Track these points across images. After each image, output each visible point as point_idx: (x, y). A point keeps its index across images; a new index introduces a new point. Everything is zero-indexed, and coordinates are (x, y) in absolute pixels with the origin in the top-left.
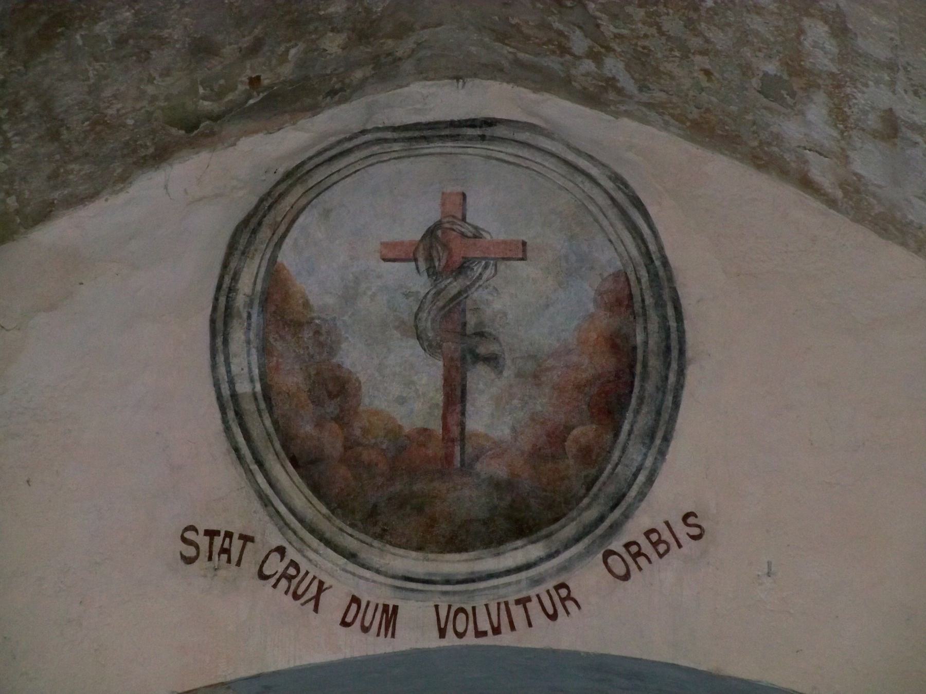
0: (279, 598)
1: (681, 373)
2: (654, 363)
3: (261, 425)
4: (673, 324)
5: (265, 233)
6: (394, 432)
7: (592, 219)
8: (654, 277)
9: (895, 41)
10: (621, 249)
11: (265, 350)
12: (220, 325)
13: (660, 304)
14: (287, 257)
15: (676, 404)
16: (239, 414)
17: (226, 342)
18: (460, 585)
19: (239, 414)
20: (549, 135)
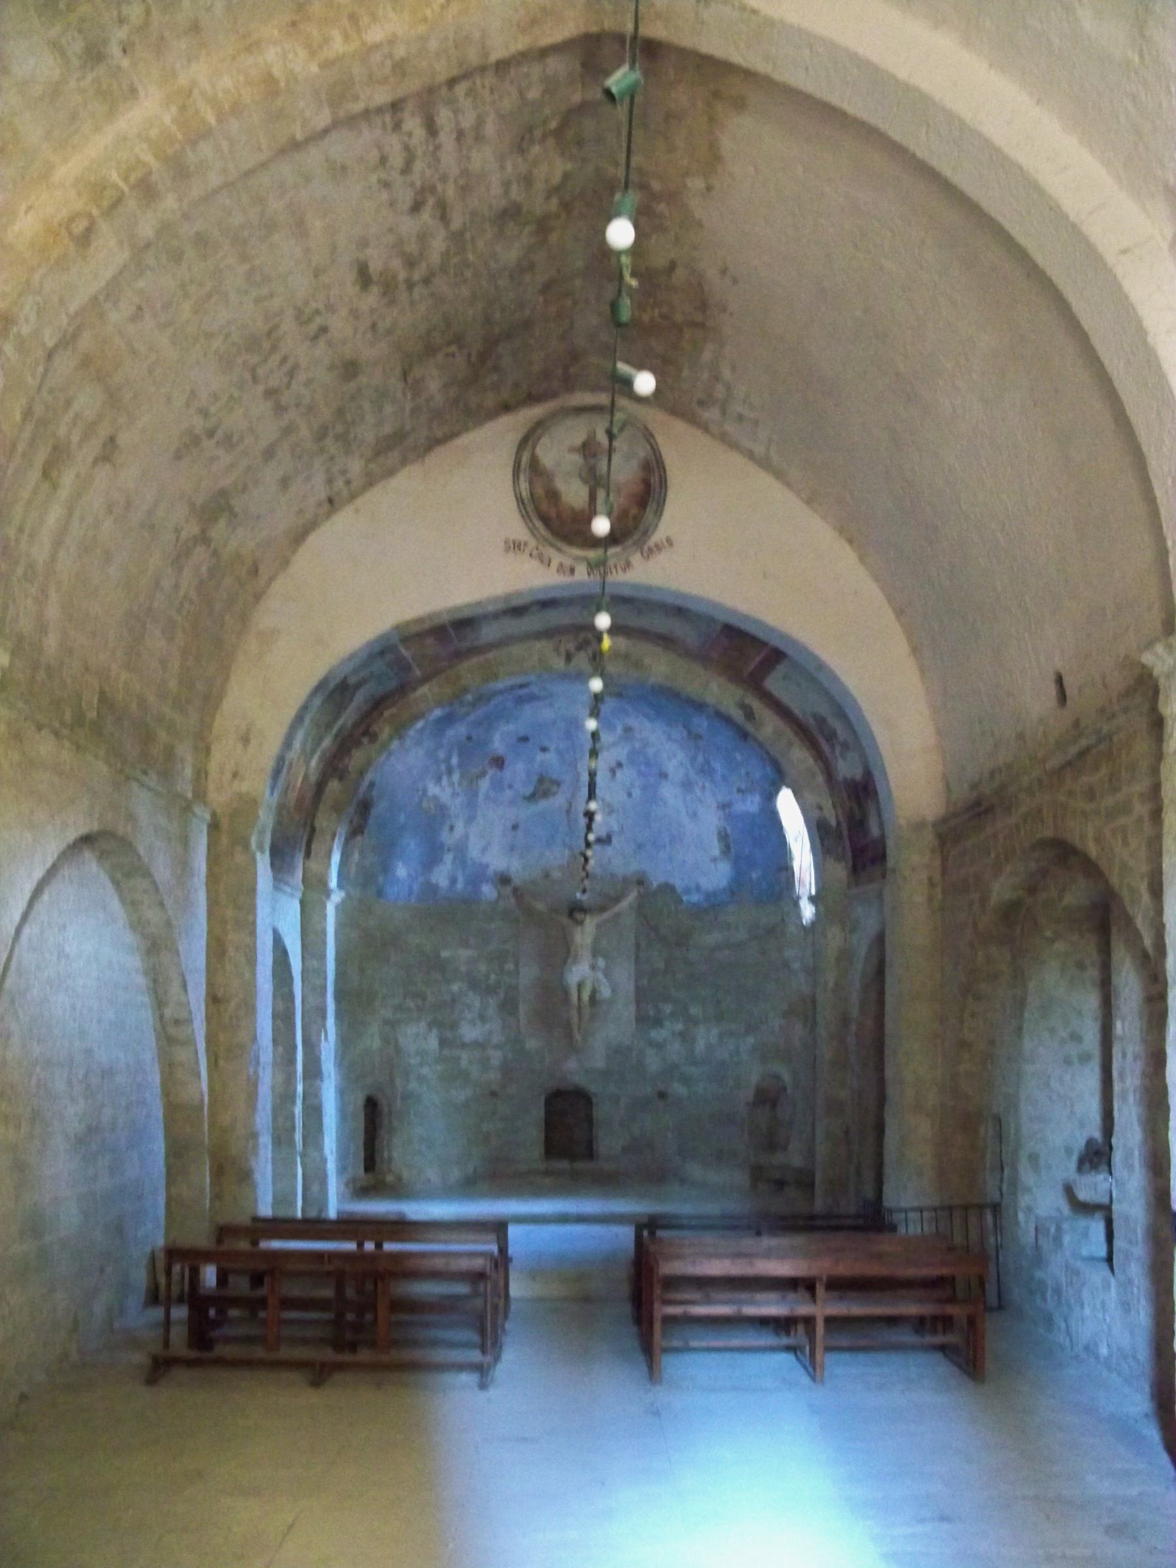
0: (535, 563)
1: (665, 493)
2: (657, 490)
3: (530, 508)
4: (662, 473)
5: (530, 443)
6: (573, 509)
7: (999, 1178)
8: (658, 463)
9: (220, 966)
10: (890, 1217)
11: (531, 482)
12: (516, 473)
13: (659, 468)
14: (539, 451)
15: (664, 501)
16: (523, 504)
17: (518, 480)
18: (334, 917)
19: (523, 504)
20: (1001, 1236)
